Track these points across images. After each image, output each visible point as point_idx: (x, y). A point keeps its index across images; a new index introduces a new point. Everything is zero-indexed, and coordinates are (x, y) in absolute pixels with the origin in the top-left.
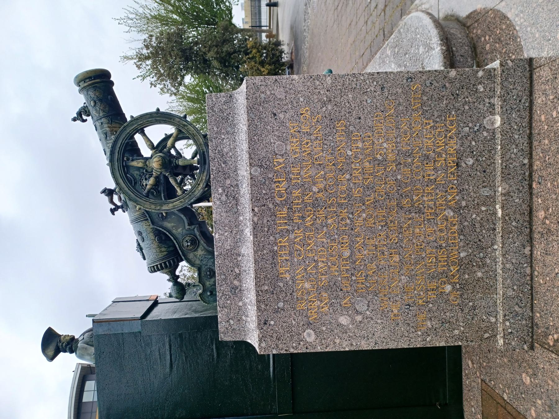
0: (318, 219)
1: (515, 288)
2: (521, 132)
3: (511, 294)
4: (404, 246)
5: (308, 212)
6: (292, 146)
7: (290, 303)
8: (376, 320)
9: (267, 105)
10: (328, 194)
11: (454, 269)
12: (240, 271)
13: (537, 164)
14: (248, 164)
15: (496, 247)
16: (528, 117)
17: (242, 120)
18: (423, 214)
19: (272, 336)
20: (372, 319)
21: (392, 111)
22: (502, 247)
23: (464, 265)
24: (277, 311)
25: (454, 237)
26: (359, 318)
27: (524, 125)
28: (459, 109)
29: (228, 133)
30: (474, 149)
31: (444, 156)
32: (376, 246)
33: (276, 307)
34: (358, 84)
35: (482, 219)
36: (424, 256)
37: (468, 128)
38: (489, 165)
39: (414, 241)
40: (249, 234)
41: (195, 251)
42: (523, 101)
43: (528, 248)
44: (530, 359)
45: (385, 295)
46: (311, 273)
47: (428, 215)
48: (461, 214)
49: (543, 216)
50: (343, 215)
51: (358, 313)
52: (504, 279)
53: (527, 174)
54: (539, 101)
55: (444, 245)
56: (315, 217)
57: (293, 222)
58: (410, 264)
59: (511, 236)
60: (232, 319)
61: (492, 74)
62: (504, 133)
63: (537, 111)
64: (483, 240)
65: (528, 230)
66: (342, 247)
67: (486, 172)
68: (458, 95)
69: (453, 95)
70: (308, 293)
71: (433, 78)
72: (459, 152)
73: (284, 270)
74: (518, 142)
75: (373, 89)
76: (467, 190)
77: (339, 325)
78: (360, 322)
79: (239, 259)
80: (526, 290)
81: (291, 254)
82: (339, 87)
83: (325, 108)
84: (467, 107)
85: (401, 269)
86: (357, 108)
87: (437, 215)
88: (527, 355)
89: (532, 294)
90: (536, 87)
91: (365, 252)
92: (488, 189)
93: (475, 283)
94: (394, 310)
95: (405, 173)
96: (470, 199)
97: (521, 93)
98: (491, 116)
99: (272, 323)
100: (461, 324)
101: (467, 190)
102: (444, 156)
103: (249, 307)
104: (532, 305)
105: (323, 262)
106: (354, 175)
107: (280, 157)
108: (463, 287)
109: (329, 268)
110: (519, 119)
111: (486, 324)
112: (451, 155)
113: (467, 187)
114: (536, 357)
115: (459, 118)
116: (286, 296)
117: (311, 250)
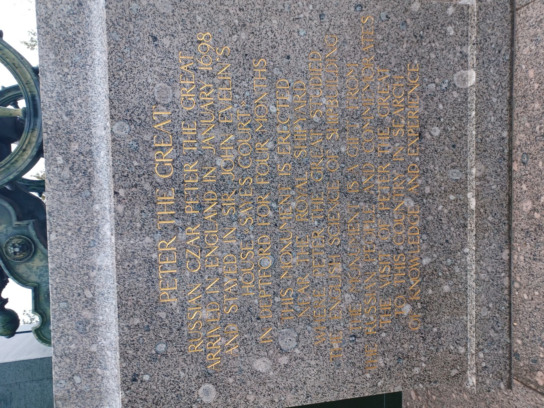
0: (224, 210)
1: (491, 305)
2: (500, 94)
3: (486, 314)
4: (349, 249)
5: (209, 197)
6: (184, 92)
7: (177, 344)
8: (309, 361)
9: (142, 22)
10: (241, 170)
11: (414, 282)
12: (93, 294)
13: (520, 138)
14: (109, 117)
15: (466, 250)
16: (508, 75)
17: (100, 45)
18: (375, 203)
19: (145, 400)
20: (303, 359)
21: (335, 51)
22: (476, 251)
23: (427, 276)
24: (154, 358)
25: (415, 237)
26: (284, 360)
27: (503, 84)
28: (423, 58)
29: (74, 64)
30: (442, 115)
31: (403, 121)
32: (310, 250)
33: (154, 352)
34: (287, 6)
35: (450, 212)
36: (375, 263)
37: (434, 85)
38: (459, 138)
39: (363, 242)
40: (109, 233)
41: (28, 261)
42: (503, 52)
43: (507, 252)
44: (505, 400)
45: (322, 323)
46: (212, 295)
47: (381, 206)
48: (424, 204)
49: (529, 208)
50: (264, 203)
51: (282, 352)
52: (478, 294)
53: (506, 151)
54: (526, 51)
55: (402, 248)
56: (219, 206)
57: (184, 214)
58: (357, 276)
59: (487, 235)
60: (78, 374)
61: (466, 13)
62: (480, 94)
63: (521, 65)
64: (451, 241)
65: (507, 227)
66: (261, 252)
67: (457, 145)
68: (422, 37)
69: (416, 37)
70: (207, 326)
71: (390, 10)
72: (423, 117)
73: (167, 291)
74: (496, 107)
75: (307, 16)
76: (432, 171)
77: (254, 373)
78: (286, 366)
79: (93, 274)
80: (503, 308)
81: (180, 265)
82: (258, 7)
83: (236, 36)
84: (433, 56)
85: (345, 283)
86: (284, 42)
87: (393, 205)
88: (499, 394)
89: (510, 313)
90: (520, 33)
91: (295, 260)
92: (458, 171)
93: (440, 301)
94: (334, 344)
95: (351, 144)
96: (435, 184)
97: (501, 41)
98: (462, 71)
99: (146, 378)
100: (423, 359)
101: (432, 171)
102: (403, 121)
103: (109, 353)
104: (510, 328)
105: (231, 276)
106: (279, 143)
107: (163, 108)
108: (425, 306)
109: (241, 284)
110: (498, 77)
111: (453, 357)
112: (412, 120)
113: (432, 166)
114: (514, 398)
115: (423, 70)
116: (171, 333)
117: (213, 258)
